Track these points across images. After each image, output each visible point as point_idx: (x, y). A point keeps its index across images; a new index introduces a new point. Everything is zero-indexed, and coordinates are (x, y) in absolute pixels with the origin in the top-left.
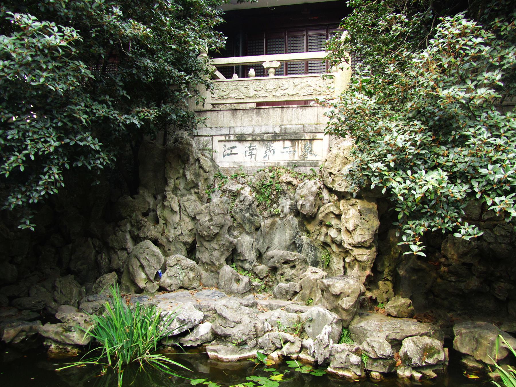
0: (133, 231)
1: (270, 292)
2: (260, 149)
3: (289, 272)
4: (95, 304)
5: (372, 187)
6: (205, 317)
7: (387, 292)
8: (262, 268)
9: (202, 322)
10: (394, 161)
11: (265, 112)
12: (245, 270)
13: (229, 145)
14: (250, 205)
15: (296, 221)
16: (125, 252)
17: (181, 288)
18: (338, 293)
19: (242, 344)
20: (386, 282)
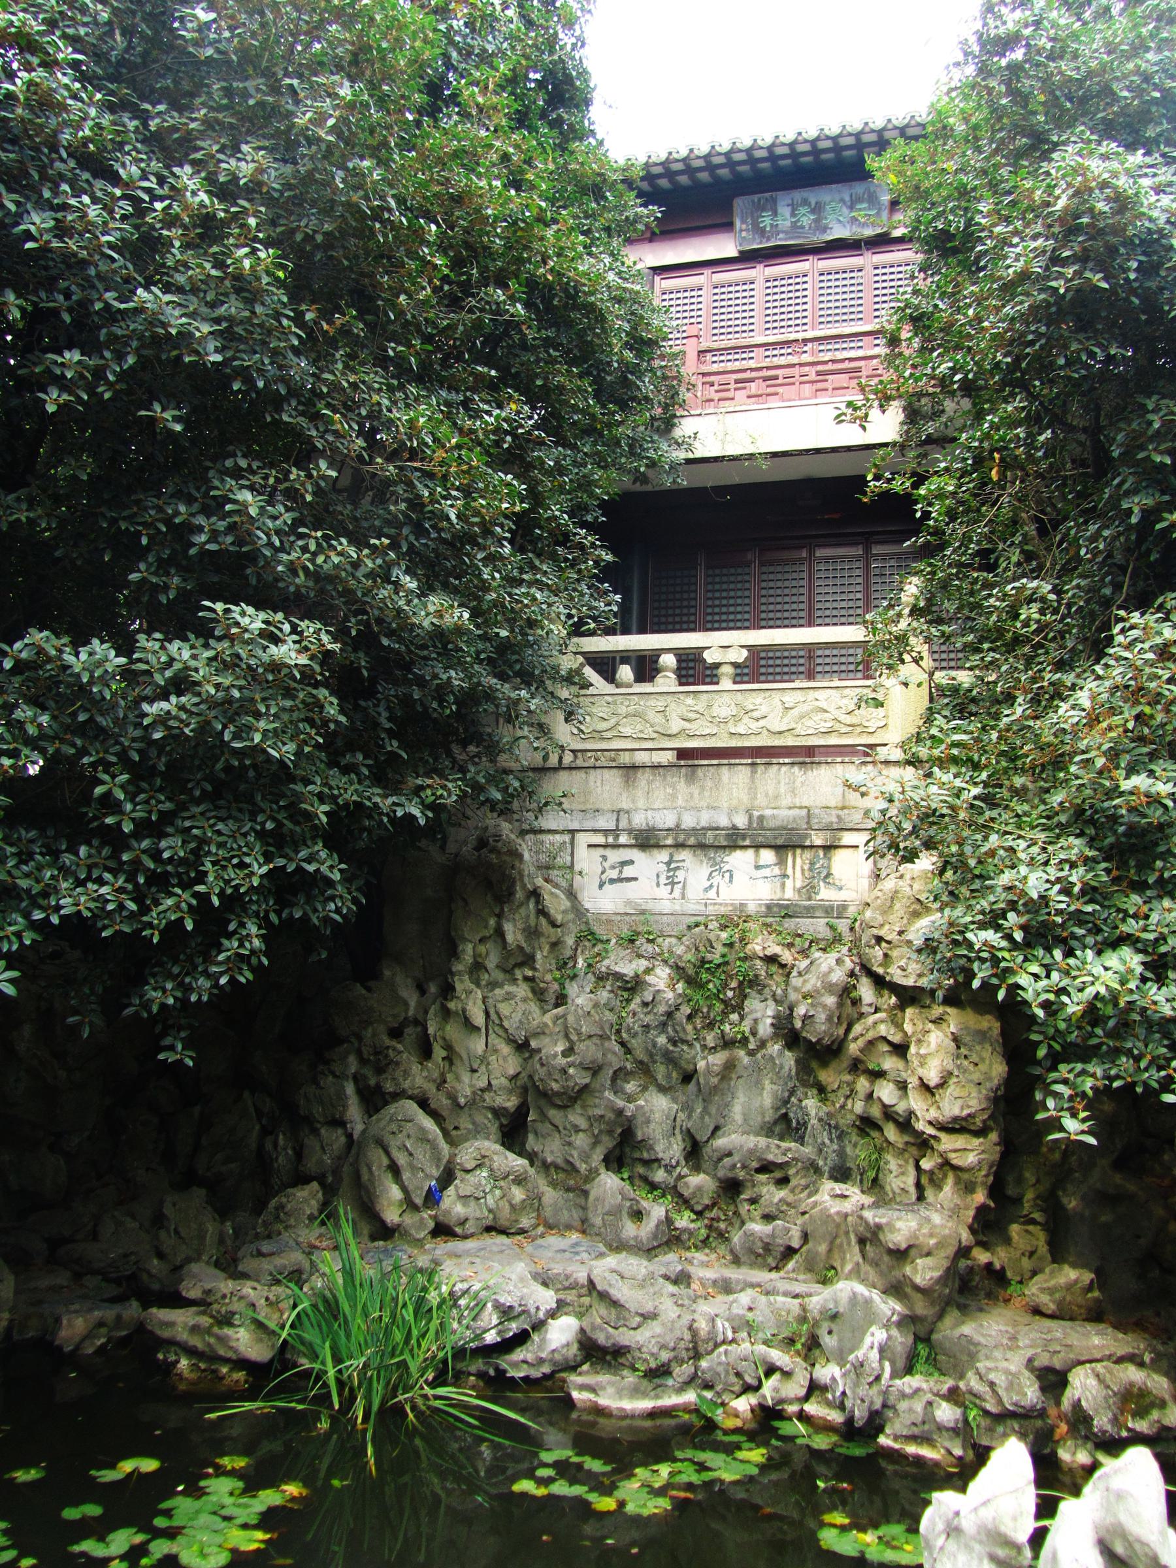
0: (365, 1078)
1: (722, 1250)
2: (695, 871)
3: (772, 1195)
4: (279, 1261)
5: (976, 984)
6: (561, 1304)
7: (1032, 1254)
8: (698, 1182)
9: (553, 1314)
10: (1023, 927)
11: (707, 771)
12: (653, 1186)
13: (614, 856)
14: (669, 1014)
15: (789, 1060)
16: (340, 1131)
17: (489, 1229)
18: (903, 1246)
19: (658, 1374)
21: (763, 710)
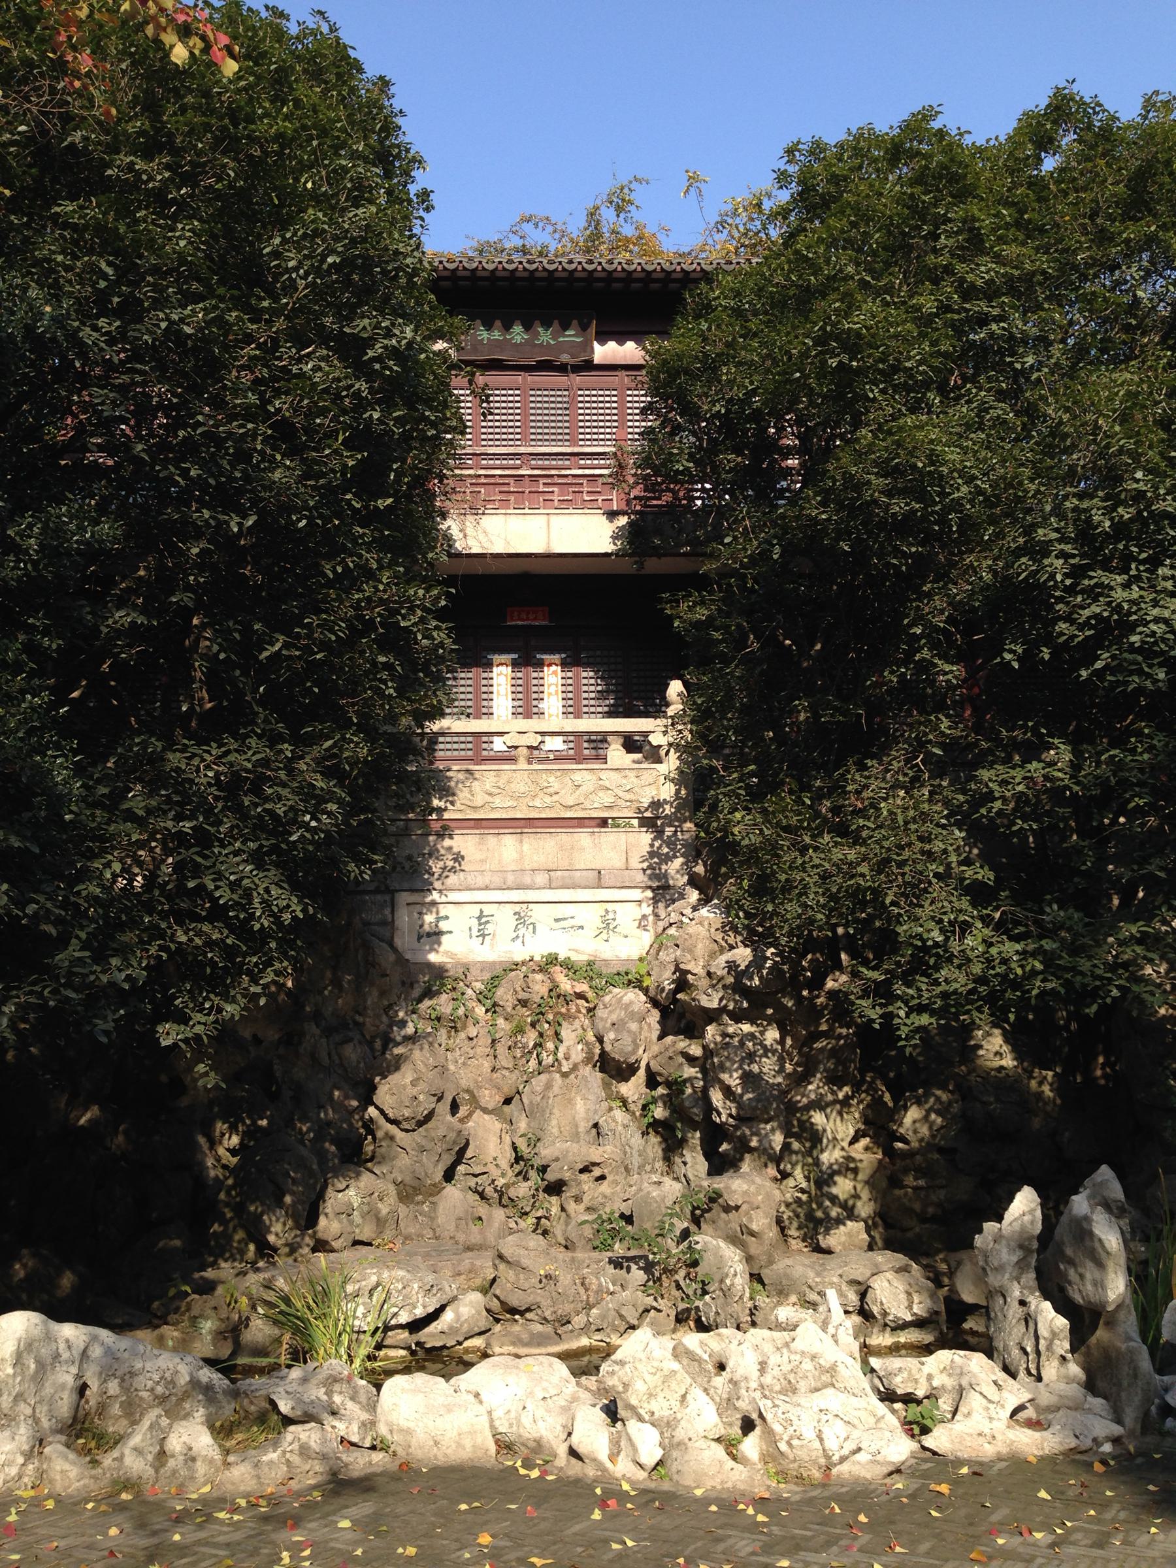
21: (556, 786)
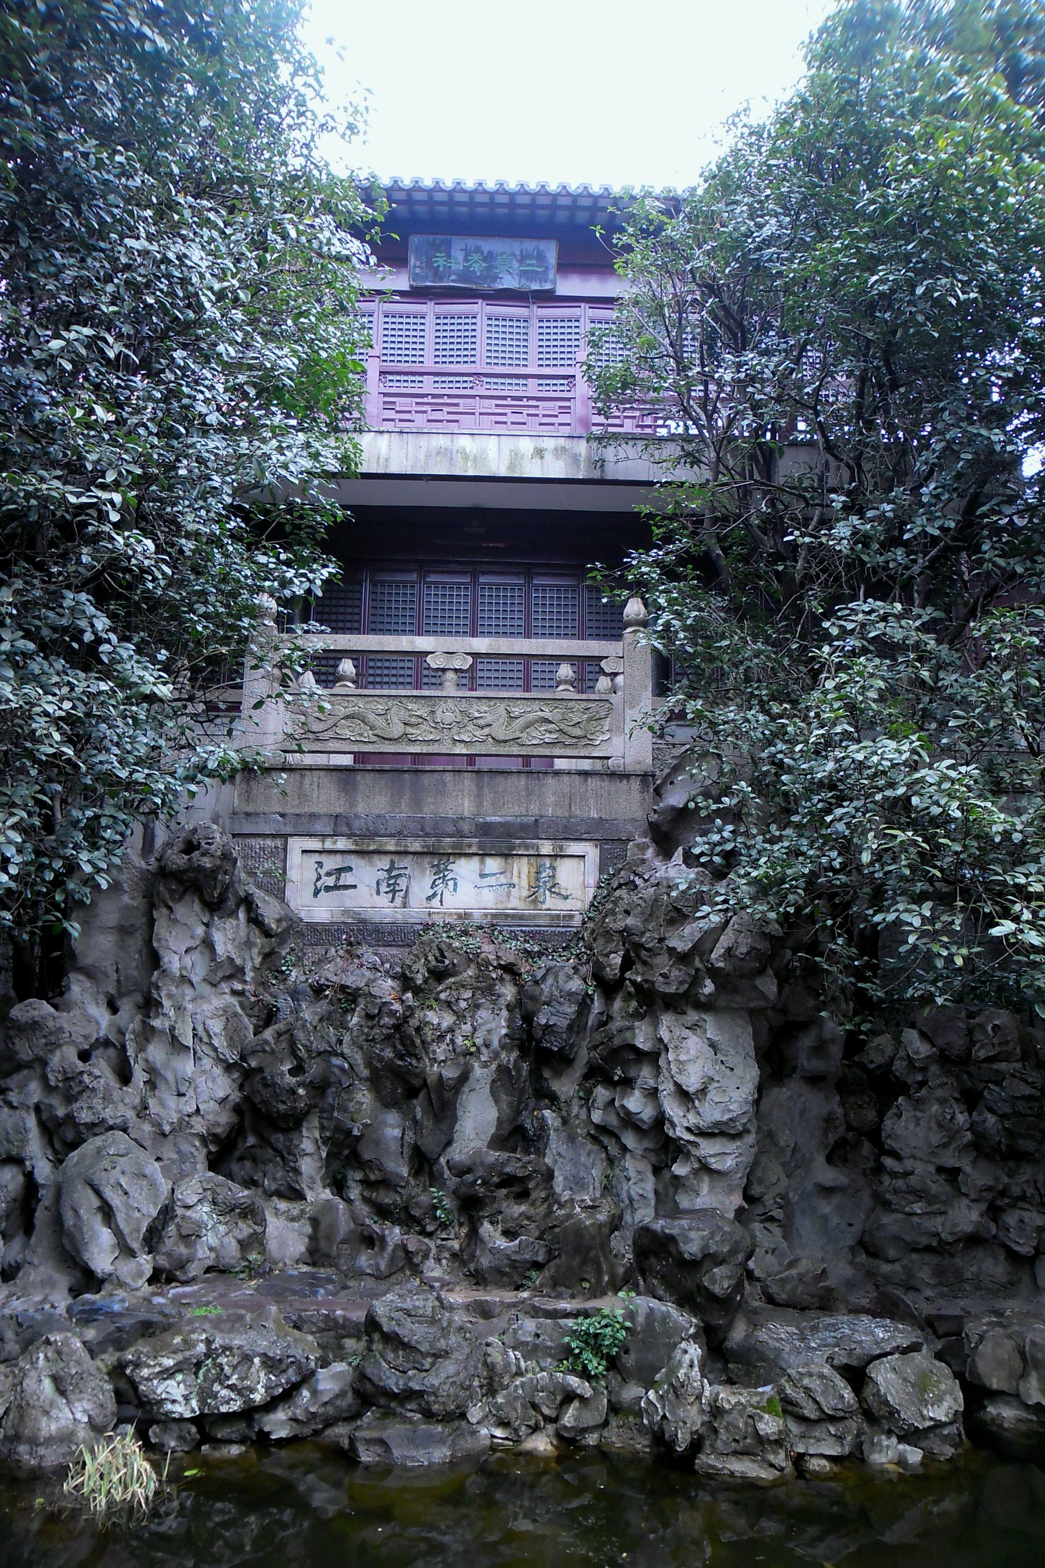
20: (768, 1225)
21: (489, 718)
